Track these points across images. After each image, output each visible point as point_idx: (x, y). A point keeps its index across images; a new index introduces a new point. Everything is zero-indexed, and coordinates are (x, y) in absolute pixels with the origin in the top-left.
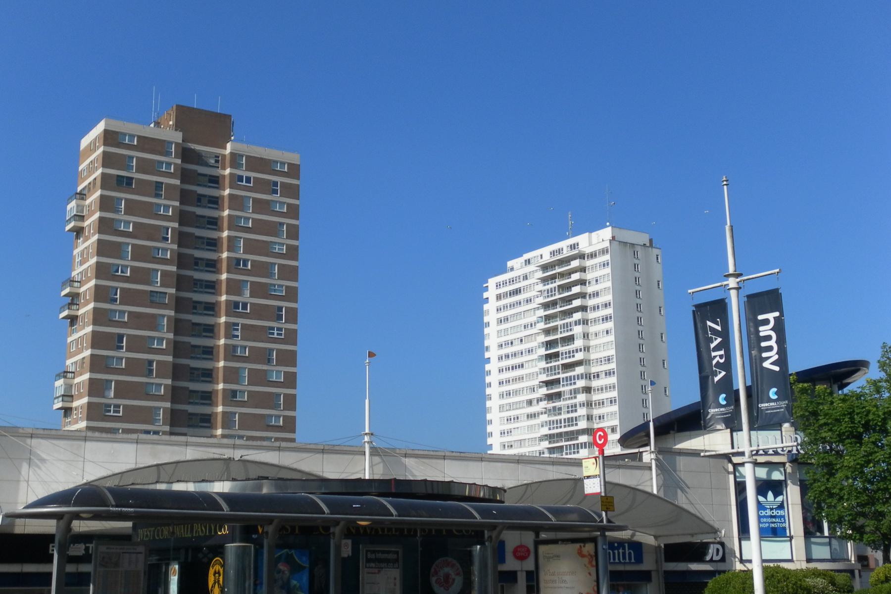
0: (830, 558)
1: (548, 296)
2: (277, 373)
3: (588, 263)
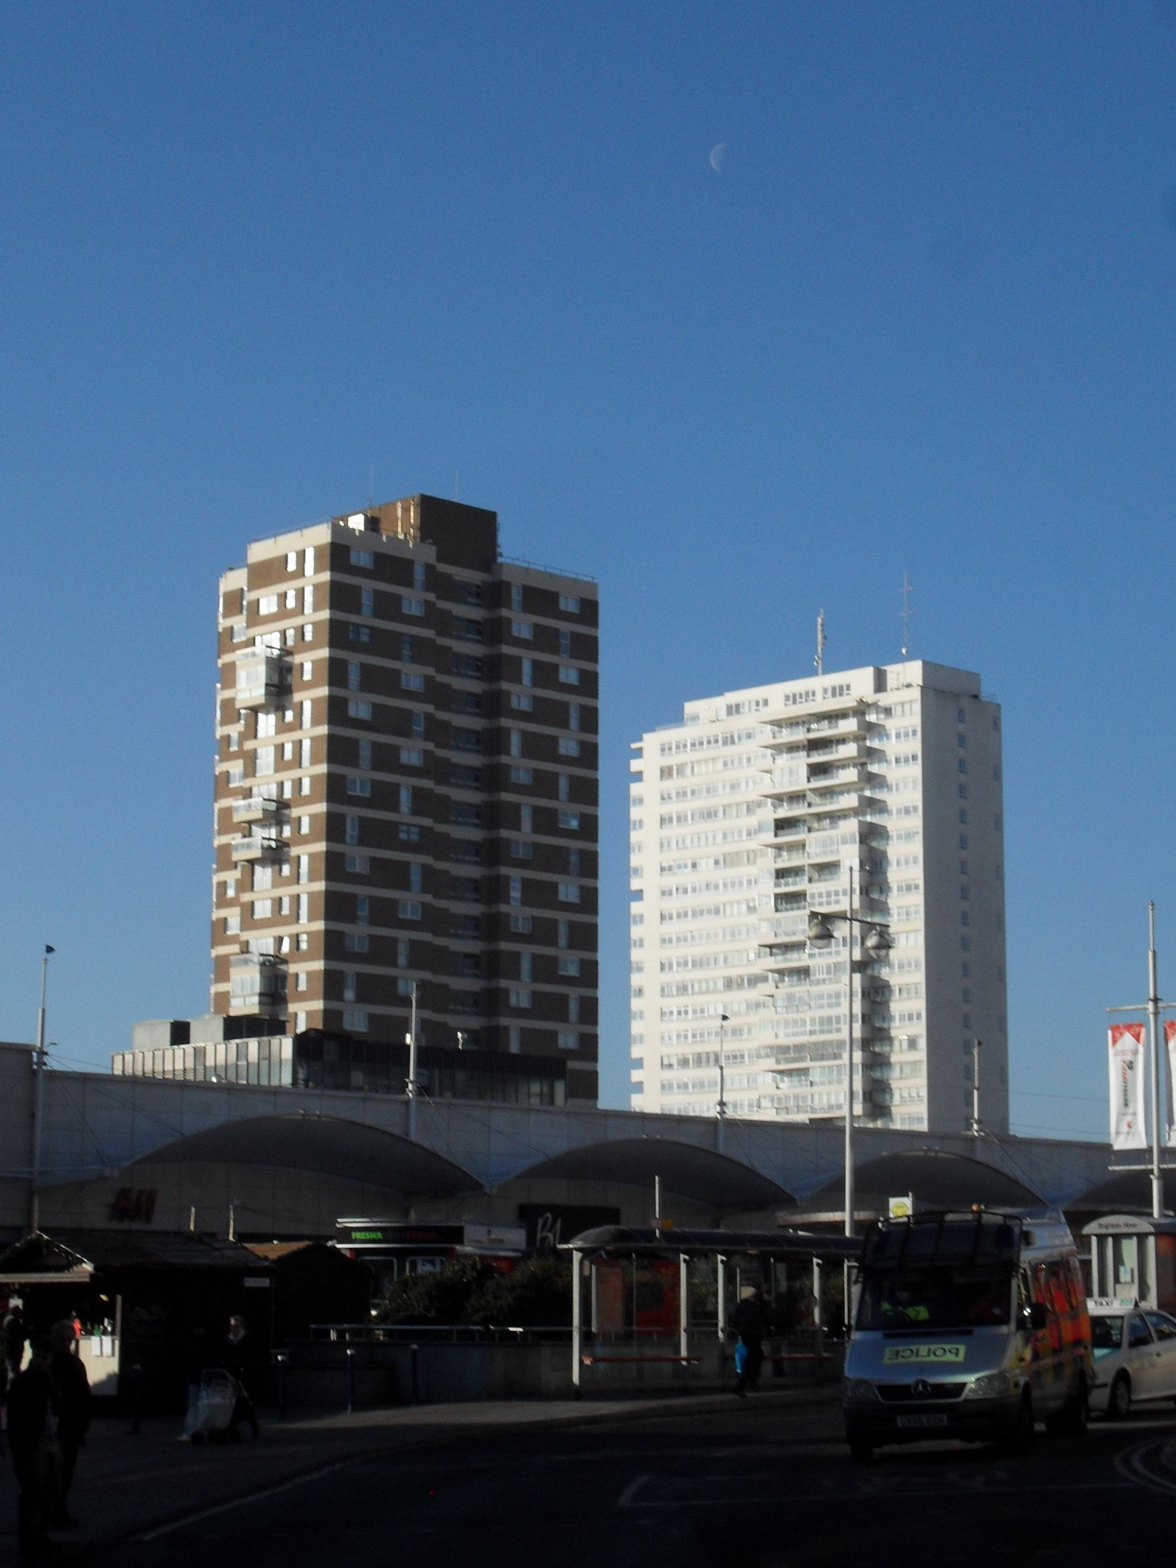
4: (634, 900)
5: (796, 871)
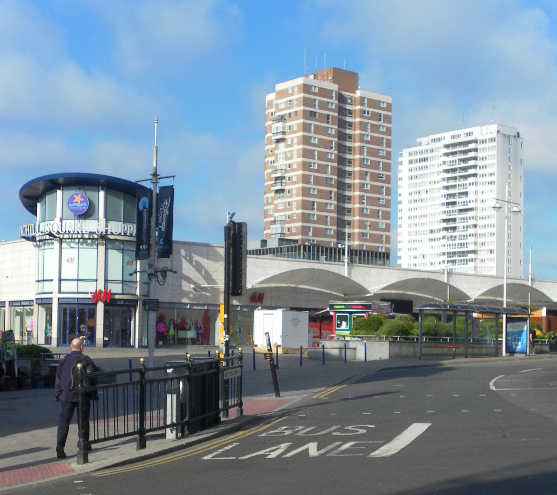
0: (148, 353)
1: (450, 165)
2: (382, 223)
3: (480, 146)
4: (399, 259)
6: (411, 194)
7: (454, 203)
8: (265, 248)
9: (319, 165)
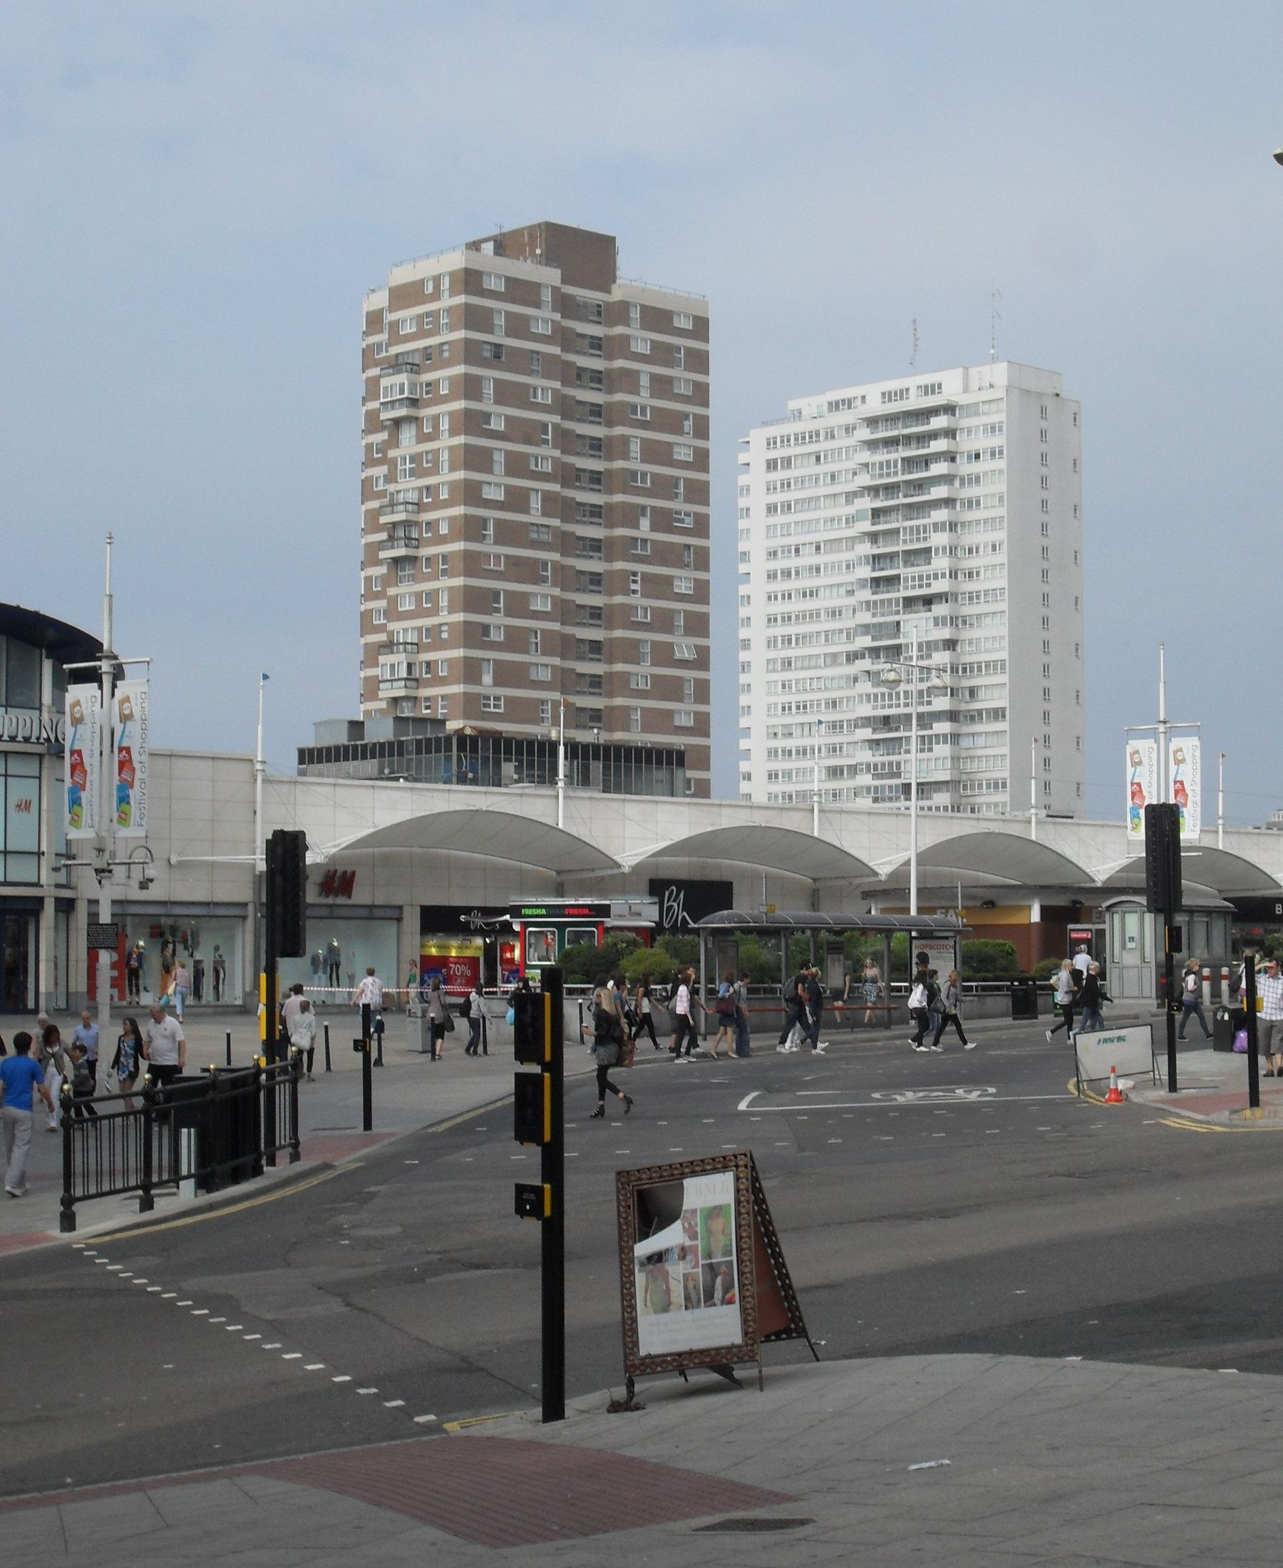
2: (684, 647)
5: (891, 557)
6: (773, 554)
7: (893, 581)
8: (358, 743)
9: (509, 490)
